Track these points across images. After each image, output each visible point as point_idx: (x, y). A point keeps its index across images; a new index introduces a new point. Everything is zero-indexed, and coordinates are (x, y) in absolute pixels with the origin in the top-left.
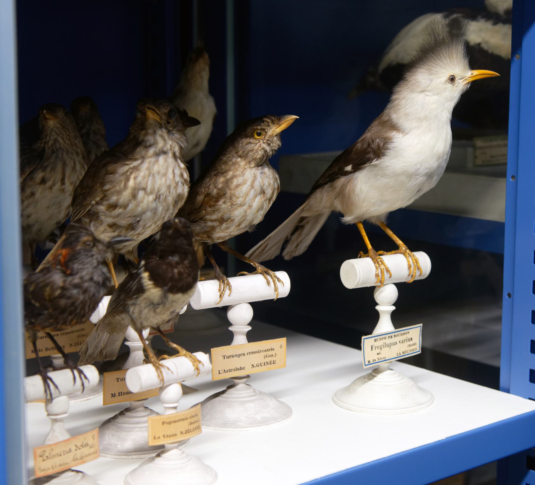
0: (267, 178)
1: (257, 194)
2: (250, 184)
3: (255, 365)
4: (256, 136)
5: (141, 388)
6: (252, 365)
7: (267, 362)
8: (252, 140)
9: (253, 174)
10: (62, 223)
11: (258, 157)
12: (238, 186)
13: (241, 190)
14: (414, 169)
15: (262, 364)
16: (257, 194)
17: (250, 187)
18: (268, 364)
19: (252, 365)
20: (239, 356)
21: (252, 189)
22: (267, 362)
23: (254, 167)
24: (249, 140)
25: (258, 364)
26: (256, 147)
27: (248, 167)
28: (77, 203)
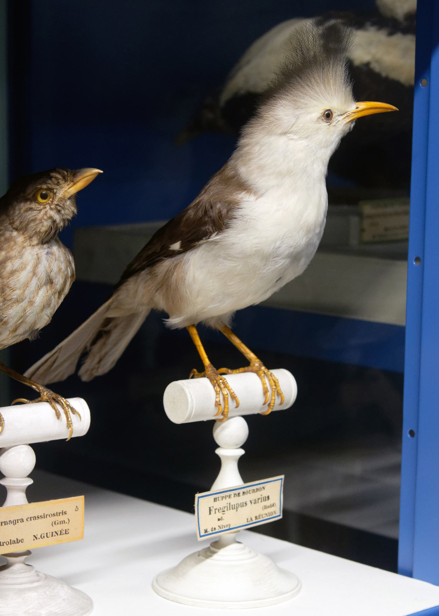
0: (56, 261)
3: (39, 536)
4: (40, 200)
6: (34, 536)
7: (56, 532)
9: (36, 256)
12: (13, 273)
15: (48, 534)
18: (57, 534)
19: (34, 536)
20: (15, 522)
22: (56, 532)
23: (38, 244)
24: (30, 205)
25: (43, 535)
27: (29, 244)
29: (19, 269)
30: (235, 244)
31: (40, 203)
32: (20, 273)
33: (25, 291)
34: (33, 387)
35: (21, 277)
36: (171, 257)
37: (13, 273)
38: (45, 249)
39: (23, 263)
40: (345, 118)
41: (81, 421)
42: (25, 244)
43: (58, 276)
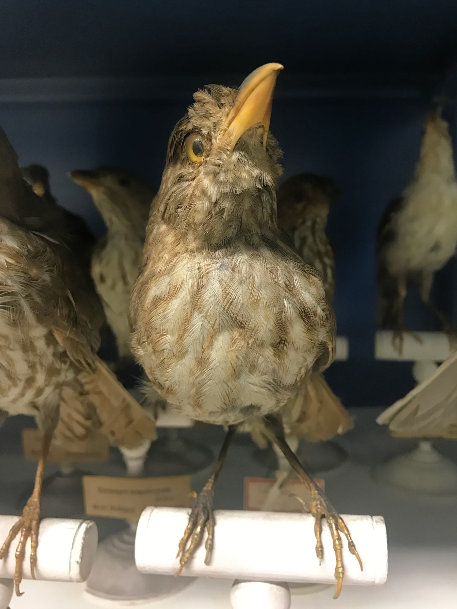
0: (240, 283)
1: (216, 326)
2: (188, 298)
4: (194, 158)
5: (153, 511)
8: (187, 170)
9: (197, 271)
10: (50, 273)
11: (199, 217)
12: (157, 301)
13: (165, 313)
14: (265, 154)
16: (216, 326)
17: (188, 307)
21: (196, 314)
23: (200, 249)
24: (180, 169)
26: (189, 192)
27: (184, 249)
28: (14, 258)
29: (165, 295)
30: (161, 270)
31: (192, 163)
32: (167, 304)
33: (181, 337)
34: (197, 527)
35: (168, 311)
36: (166, 165)
37: (157, 301)
38: (218, 259)
39: (172, 284)
40: (226, 392)
41: (362, 570)
42: (178, 249)
43: (253, 314)
